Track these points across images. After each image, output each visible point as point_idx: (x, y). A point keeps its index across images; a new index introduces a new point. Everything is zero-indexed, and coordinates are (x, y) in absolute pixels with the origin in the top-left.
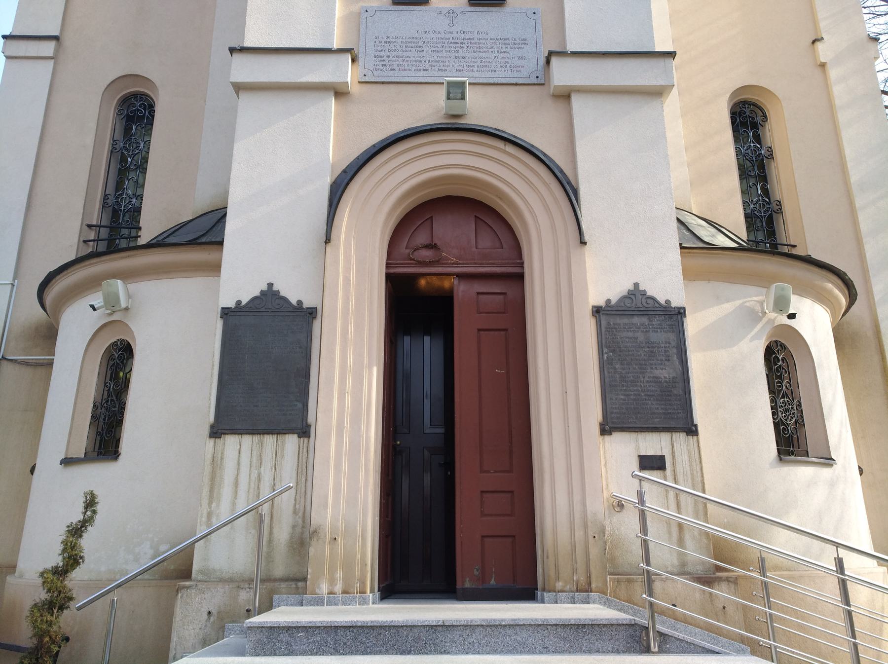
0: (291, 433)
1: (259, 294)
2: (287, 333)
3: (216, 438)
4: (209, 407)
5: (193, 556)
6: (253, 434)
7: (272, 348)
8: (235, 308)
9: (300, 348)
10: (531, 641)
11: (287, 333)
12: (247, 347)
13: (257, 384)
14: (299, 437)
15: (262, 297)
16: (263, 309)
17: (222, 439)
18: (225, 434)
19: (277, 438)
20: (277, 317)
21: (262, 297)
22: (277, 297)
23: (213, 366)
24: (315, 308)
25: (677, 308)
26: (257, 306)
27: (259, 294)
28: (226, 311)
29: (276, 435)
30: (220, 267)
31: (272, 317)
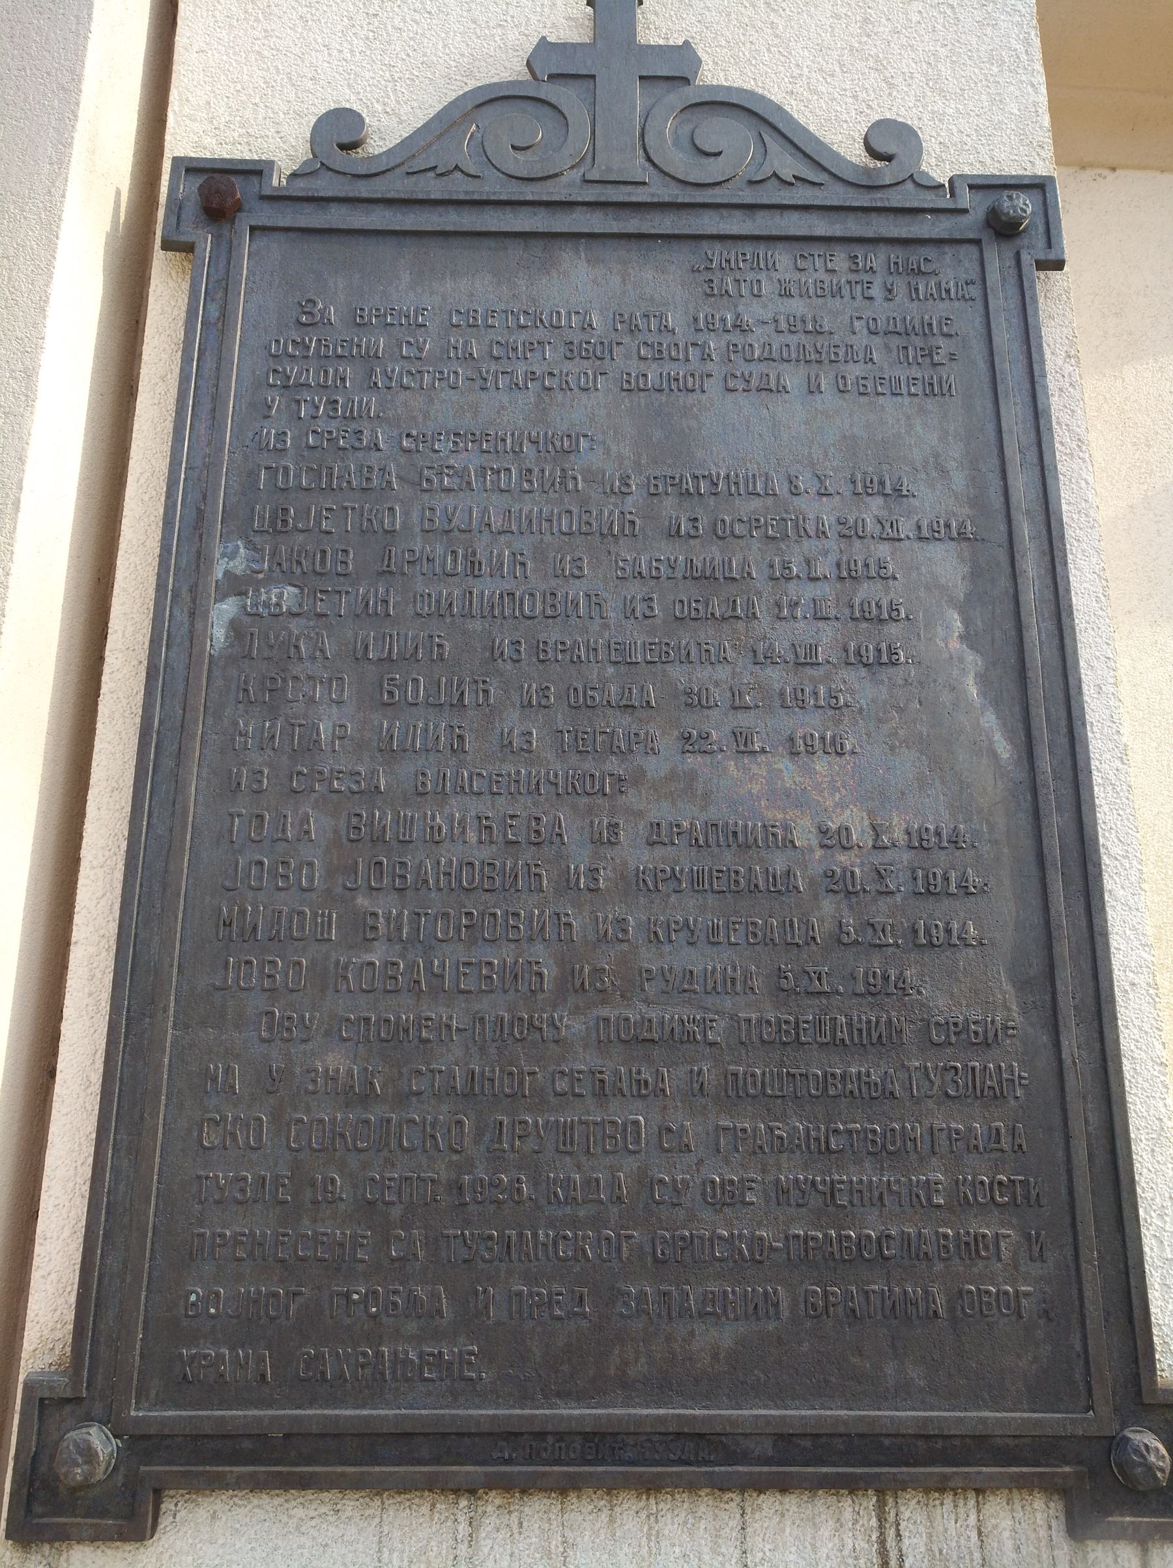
21: (549, 92)
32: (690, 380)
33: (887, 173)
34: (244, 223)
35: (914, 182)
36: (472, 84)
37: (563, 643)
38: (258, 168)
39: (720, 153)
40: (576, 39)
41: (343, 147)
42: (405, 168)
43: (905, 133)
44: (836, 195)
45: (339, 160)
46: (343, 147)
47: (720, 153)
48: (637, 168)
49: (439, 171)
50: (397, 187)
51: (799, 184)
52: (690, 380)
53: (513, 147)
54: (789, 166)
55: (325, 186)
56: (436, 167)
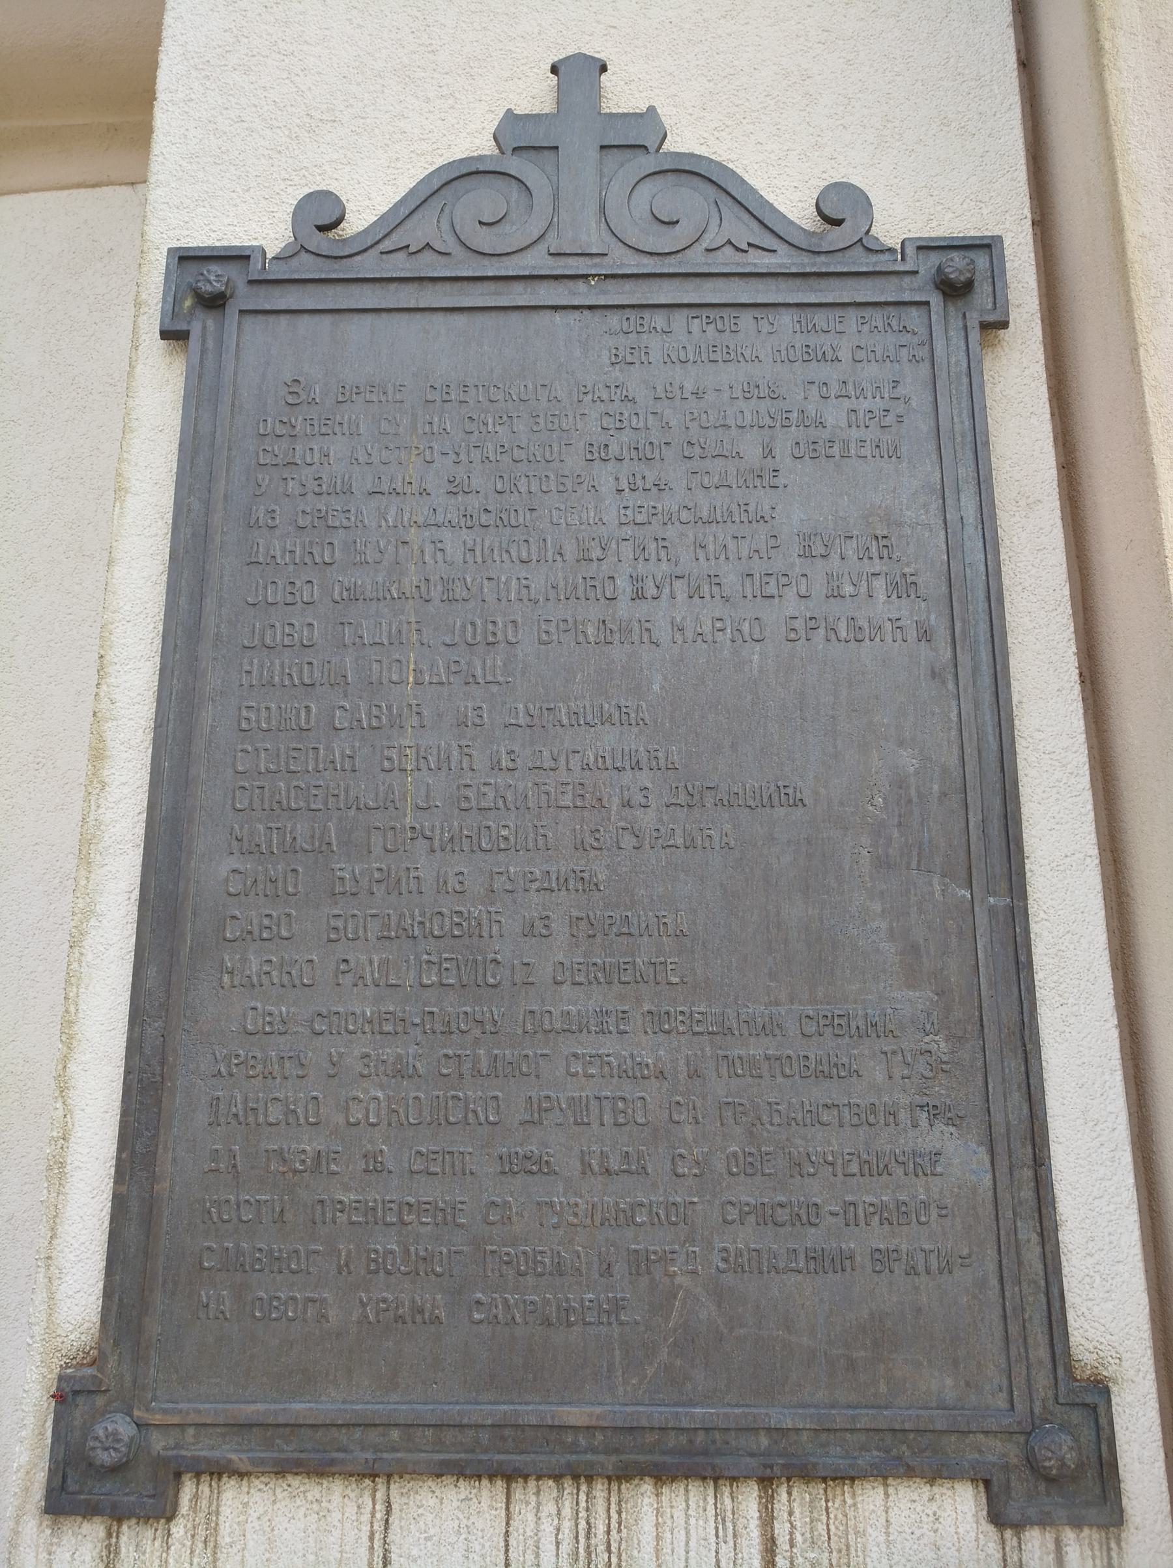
0: (909, 1473)
1: (484, 145)
2: (769, 453)
3: (118, 1515)
4: (57, 1170)
5: (152, 67)
6: (510, 1476)
7: (639, 596)
8: (298, 249)
9: (904, 587)
10: (169, 299)
11: (769, 453)
12: (412, 578)
13: (529, 931)
14: (997, 1518)
15: (514, 165)
16: (535, 261)
17: (178, 1529)
18: (218, 1471)
19: (767, 1521)
20: (658, 320)
21: (514, 165)
22: (648, 163)
23: (98, 755)
24: (988, 246)
25: (926, 247)
26: (484, 240)
27: (484, 145)
28: (214, 278)
29: (749, 1499)
30: (145, 97)
31: (614, 320)
32: (791, 351)
33: (837, 237)
34: (232, 310)
35: (307, 251)
36: (440, 162)
37: (237, 1056)
38: (247, 253)
39: (677, 222)
40: (547, 110)
41: (323, 229)
42: (383, 247)
43: (859, 200)
44: (783, 260)
45: (318, 241)
46: (323, 229)
47: (677, 222)
48: (592, 237)
49: (412, 249)
50: (367, 266)
51: (751, 250)
52: (791, 351)
53: (480, 222)
54: (743, 231)
55: (308, 267)
56: (408, 246)
